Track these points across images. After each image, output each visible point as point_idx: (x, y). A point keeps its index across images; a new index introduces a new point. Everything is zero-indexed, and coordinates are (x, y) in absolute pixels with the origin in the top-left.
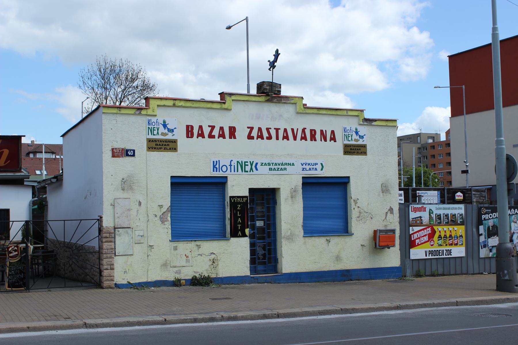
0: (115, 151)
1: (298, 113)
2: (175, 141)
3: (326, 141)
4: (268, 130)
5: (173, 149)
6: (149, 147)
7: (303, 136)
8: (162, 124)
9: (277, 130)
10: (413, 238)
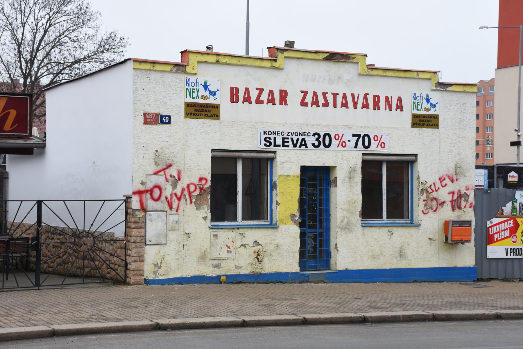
0: (148, 116)
1: (360, 75)
4: (324, 94)
5: (214, 116)
6: (187, 113)
9: (335, 95)
10: (491, 232)
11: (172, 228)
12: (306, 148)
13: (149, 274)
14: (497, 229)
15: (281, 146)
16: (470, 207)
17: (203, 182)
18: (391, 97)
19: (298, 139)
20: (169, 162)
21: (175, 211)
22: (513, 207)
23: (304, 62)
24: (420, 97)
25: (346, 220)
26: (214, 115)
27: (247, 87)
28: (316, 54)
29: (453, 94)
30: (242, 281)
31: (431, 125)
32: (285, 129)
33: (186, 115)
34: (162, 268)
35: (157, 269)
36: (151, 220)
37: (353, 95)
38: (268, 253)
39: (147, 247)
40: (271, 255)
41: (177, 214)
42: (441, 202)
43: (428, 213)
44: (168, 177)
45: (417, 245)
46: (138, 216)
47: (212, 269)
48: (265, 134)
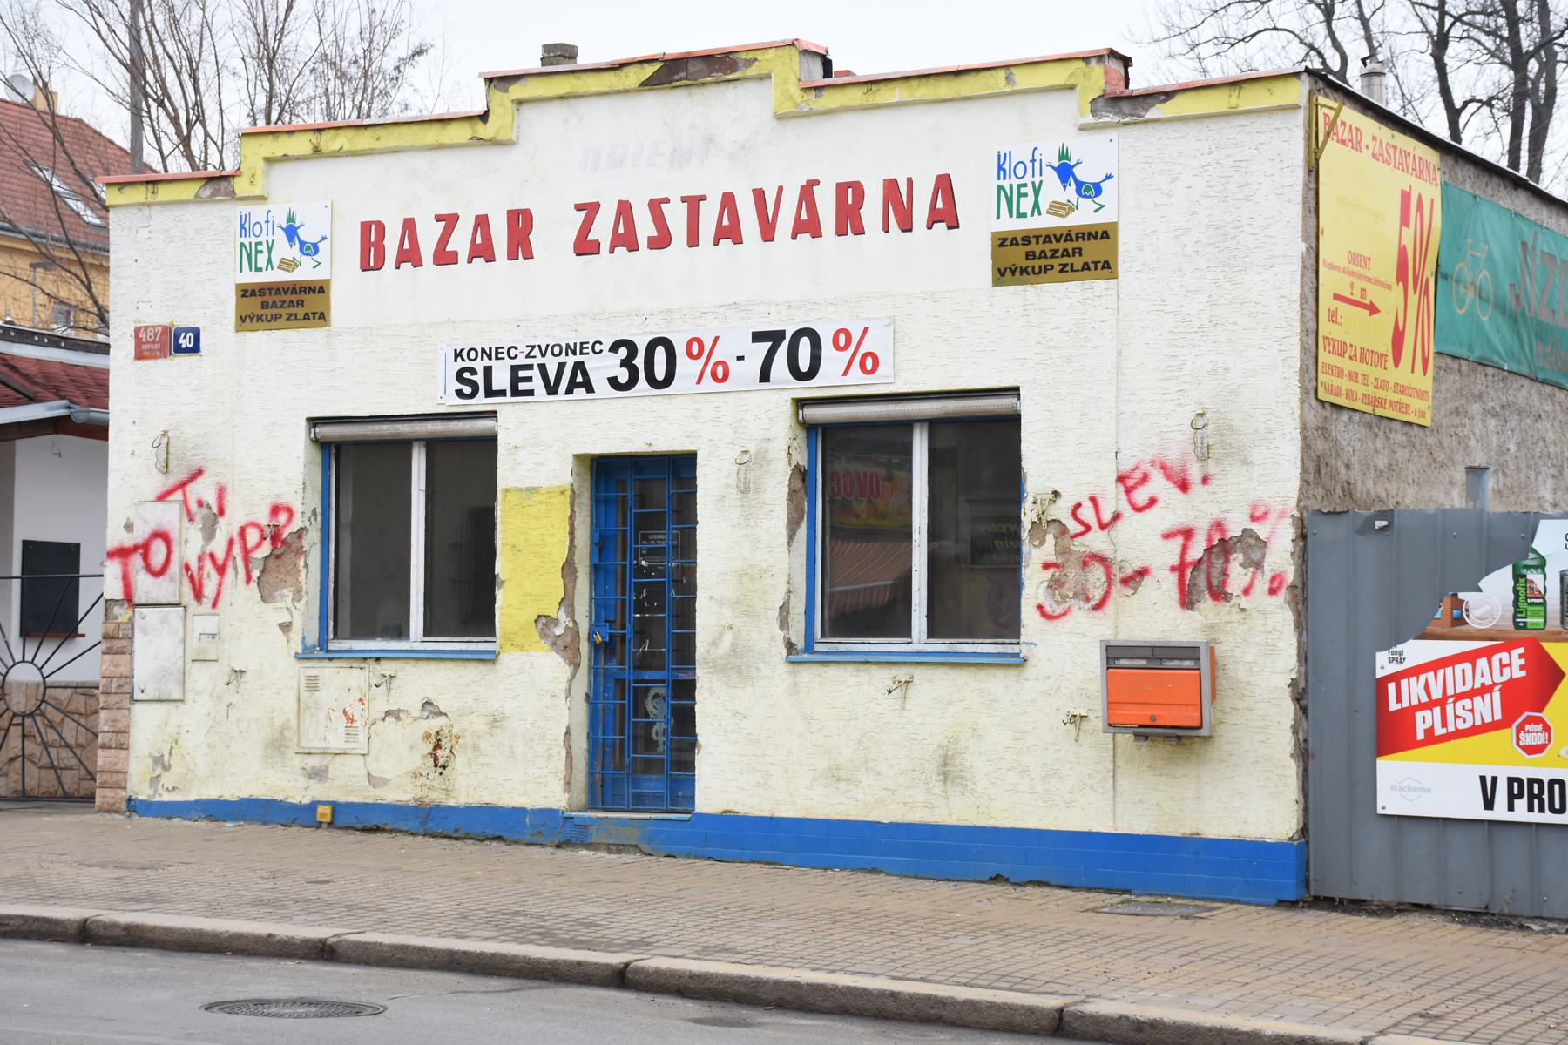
0: (144, 336)
1: (781, 117)
2: (1105, 232)
3: (820, 236)
4: (656, 206)
5: (1096, 269)
6: (999, 270)
7: (804, 216)
8: (1053, 168)
9: (693, 203)
10: (1399, 700)
11: (198, 654)
12: (590, 396)
13: (139, 788)
14: (1427, 688)
15: (509, 393)
16: (1273, 591)
17: (283, 517)
18: (910, 182)
19: (561, 366)
20: (195, 464)
21: (210, 605)
22: (1524, 595)
23: (583, 106)
24: (264, 225)
25: (728, 636)
26: (314, 314)
27: (409, 216)
28: (618, 72)
29: (1182, 129)
30: (381, 826)
31: (300, 316)
32: (519, 339)
33: (240, 322)
34: (172, 770)
35: (159, 771)
36: (145, 631)
37: (759, 195)
38: (467, 740)
39: (137, 708)
40: (476, 749)
41: (215, 614)
42: (1129, 571)
43: (1065, 614)
44: (193, 506)
45: (1017, 739)
46: (119, 620)
47: (302, 781)
48: (459, 359)
